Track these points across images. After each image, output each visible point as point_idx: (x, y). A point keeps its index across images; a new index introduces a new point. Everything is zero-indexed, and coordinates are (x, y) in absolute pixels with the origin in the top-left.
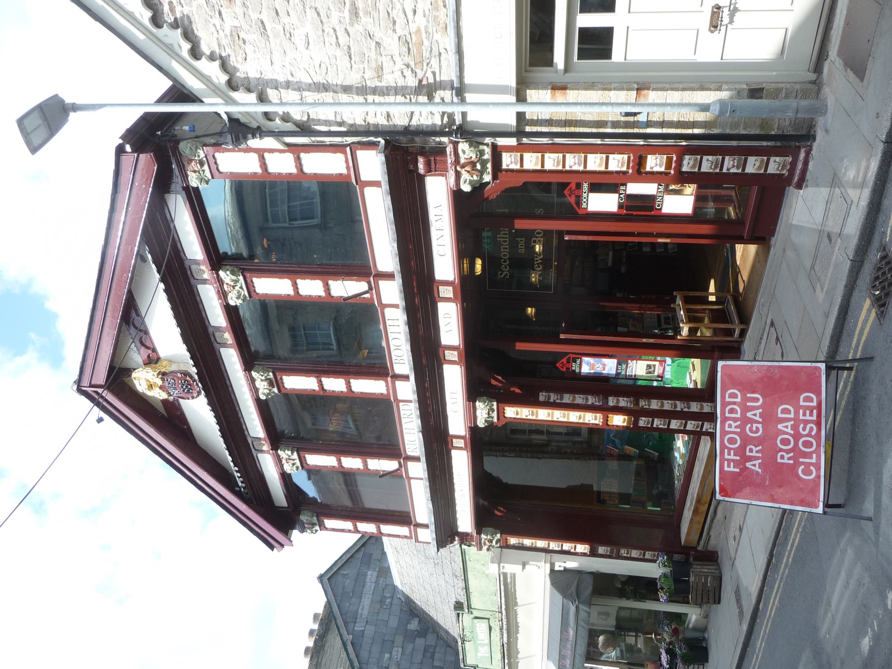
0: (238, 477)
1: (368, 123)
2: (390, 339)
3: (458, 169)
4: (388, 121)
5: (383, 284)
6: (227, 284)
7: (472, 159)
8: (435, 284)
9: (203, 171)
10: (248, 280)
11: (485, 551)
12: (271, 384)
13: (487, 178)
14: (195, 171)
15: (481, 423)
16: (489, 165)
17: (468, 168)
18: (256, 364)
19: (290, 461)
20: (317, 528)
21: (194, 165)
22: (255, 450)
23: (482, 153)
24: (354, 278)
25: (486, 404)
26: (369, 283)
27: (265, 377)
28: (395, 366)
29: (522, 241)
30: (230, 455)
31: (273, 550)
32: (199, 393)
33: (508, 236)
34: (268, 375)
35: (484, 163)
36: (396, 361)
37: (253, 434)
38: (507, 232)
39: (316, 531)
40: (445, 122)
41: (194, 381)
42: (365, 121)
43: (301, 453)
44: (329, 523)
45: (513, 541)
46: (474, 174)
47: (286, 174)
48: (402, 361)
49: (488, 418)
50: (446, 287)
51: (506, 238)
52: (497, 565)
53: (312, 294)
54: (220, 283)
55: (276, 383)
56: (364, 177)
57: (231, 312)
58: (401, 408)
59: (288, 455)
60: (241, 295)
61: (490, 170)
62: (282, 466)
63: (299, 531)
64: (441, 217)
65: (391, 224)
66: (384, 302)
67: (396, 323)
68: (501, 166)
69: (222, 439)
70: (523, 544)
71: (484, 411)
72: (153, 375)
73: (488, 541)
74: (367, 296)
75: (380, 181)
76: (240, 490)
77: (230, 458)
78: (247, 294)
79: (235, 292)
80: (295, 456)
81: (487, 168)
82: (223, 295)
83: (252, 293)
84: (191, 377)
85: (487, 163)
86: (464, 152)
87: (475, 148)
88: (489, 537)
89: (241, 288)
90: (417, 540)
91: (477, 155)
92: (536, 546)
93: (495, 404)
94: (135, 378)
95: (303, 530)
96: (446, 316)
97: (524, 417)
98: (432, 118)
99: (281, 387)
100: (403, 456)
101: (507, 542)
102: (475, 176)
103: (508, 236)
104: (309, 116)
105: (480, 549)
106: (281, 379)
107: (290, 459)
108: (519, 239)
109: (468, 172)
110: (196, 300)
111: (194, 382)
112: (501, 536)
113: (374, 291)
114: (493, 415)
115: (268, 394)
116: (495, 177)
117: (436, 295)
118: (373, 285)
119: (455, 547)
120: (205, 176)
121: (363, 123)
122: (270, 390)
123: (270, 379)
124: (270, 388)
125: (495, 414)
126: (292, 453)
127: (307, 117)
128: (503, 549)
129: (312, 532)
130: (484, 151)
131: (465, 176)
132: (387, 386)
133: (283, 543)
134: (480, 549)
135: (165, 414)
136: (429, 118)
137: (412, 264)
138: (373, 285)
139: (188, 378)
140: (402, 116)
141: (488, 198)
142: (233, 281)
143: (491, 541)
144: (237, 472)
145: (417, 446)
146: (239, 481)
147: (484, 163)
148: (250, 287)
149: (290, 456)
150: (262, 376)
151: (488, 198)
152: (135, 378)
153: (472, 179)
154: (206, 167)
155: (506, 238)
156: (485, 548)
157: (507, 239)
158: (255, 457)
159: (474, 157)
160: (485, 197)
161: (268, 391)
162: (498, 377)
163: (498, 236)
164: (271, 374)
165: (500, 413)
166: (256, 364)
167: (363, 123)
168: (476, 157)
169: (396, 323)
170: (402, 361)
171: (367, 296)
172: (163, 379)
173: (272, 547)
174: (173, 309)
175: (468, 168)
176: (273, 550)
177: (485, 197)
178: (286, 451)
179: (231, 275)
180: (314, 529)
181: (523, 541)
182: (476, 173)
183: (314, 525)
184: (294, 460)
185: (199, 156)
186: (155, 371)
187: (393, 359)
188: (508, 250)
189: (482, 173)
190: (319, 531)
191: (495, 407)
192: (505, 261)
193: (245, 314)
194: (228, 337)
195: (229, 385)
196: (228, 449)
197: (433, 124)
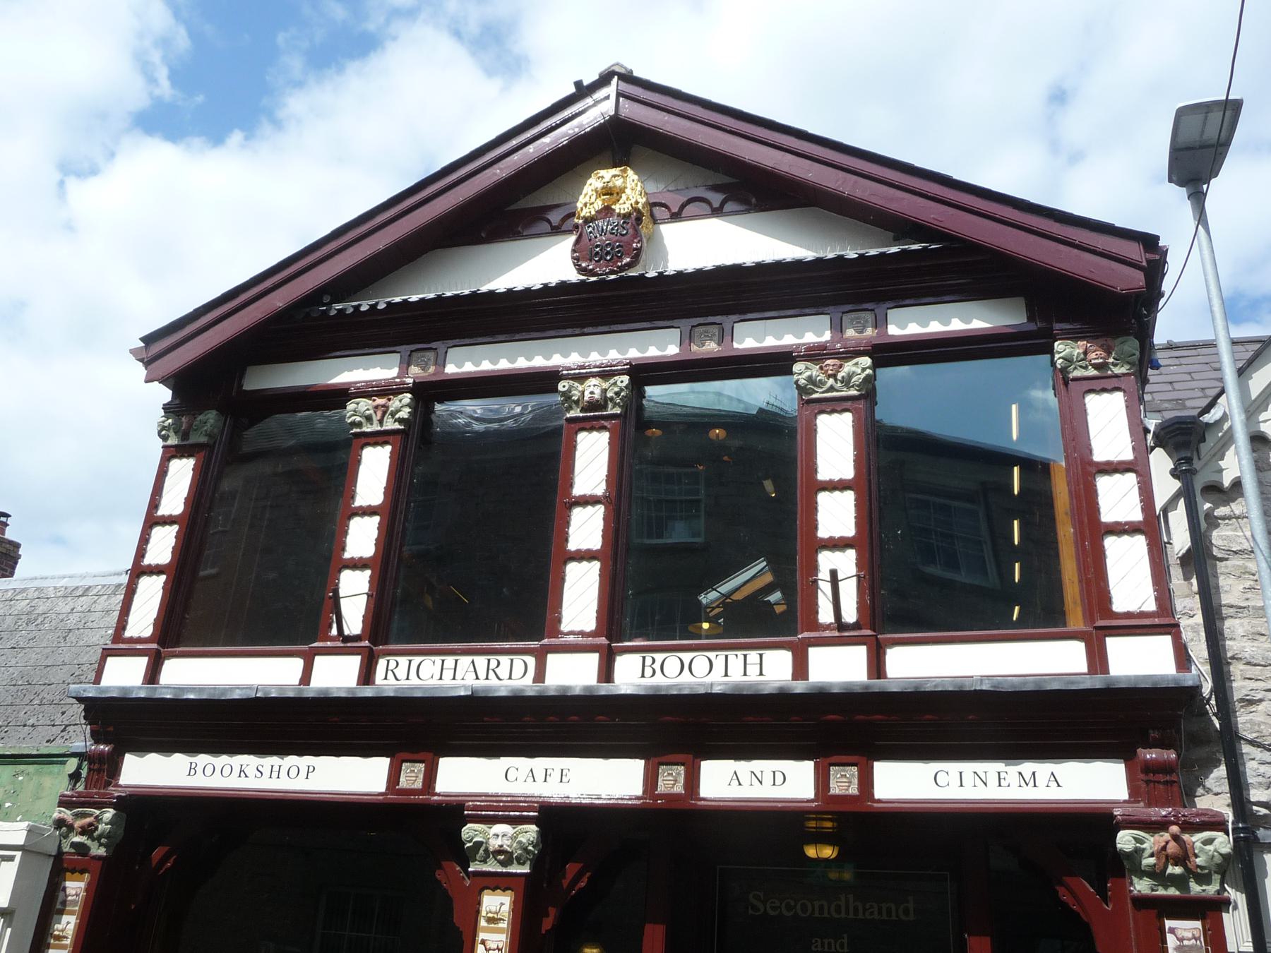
0: (360, 305)
1: (1230, 663)
2: (712, 655)
3: (1175, 829)
4: (1242, 700)
5: (354, 663)
6: (841, 366)
7: (1192, 859)
8: (691, 756)
9: (1085, 368)
10: (848, 404)
11: (56, 815)
12: (593, 406)
13: (1142, 886)
14: (1085, 353)
15: (470, 832)
16: (1173, 892)
17: (1173, 848)
18: (226, 420)
19: (379, 413)
20: (173, 441)
21: (1096, 356)
22: (412, 351)
23: (1204, 879)
24: (868, 598)
25: (530, 848)
26: (856, 626)
27: (611, 399)
28: (636, 659)
29: (842, 946)
30: (422, 300)
31: (142, 339)
32: (581, 270)
33: (851, 916)
34: (615, 405)
35: (1180, 882)
36: (649, 661)
37: (740, 328)
38: (861, 916)
39: (165, 438)
40: (1255, 808)
41: (622, 269)
42: (1233, 658)
43: (399, 437)
44: (182, 472)
45: (75, 887)
46: (1158, 859)
47: (567, 533)
48: (648, 671)
49: (486, 850)
50: (421, 776)
51: (847, 912)
52: (21, 842)
53: (348, 537)
54: (843, 353)
55: (594, 416)
56: (552, 659)
57: (340, 396)
58: (518, 661)
59: (398, 411)
60: (815, 385)
61: (1161, 892)
62: (367, 395)
63: (168, 404)
64: (1032, 783)
65: (1035, 682)
66: (319, 660)
67: (448, 674)
68: (1170, 918)
69: (466, 292)
70: (61, 912)
71: (509, 843)
72: (637, 203)
73: (91, 824)
74: (334, 632)
75: (99, 684)
76: (324, 305)
77: (414, 298)
78: (815, 396)
79: (822, 377)
80: (390, 425)
81: (1166, 888)
82: (369, 391)
83: (817, 407)
84: (630, 266)
85: (1178, 889)
86: (1209, 841)
87: (1218, 865)
88: (102, 827)
89: (832, 389)
90: (107, 653)
91: (1201, 867)
92: (48, 946)
93: (525, 869)
94: (625, 171)
95: (167, 408)
96: (311, 769)
97: (482, 936)
98: (1260, 784)
99: (582, 425)
100: (374, 648)
101: (73, 871)
102: (1152, 860)
103: (851, 916)
104: (1222, 560)
105: (64, 803)
106: (603, 428)
107: (384, 413)
108: (845, 941)
109: (1164, 848)
110: (925, 296)
111: (618, 267)
112: (94, 858)
113: (340, 644)
114: (491, 861)
115: (570, 397)
116: (1142, 902)
117: (834, 759)
118: (349, 645)
119: (81, 740)
120: (1075, 368)
121: (1229, 655)
122: (577, 402)
123: (605, 407)
124: (581, 405)
125: (492, 867)
126: (400, 421)
127: (1220, 556)
128: (51, 861)
129: (163, 428)
130: (1209, 882)
131: (1152, 842)
132: (140, 640)
133: (154, 365)
134: (64, 803)
135: (513, 207)
136: (1260, 779)
137: (927, 717)
138: (349, 645)
139: (627, 260)
140: (1257, 728)
141: (440, 867)
142: (850, 376)
143: (87, 831)
144: (373, 307)
145: (403, 682)
146: (348, 306)
147: (1180, 882)
148: (378, 438)
149: (393, 414)
150: (617, 394)
151: (440, 867)
152: (625, 171)
153: (1146, 854)
154: (1092, 372)
155: (847, 912)
156: (67, 814)
157: (843, 915)
158: (711, 319)
159: (1199, 861)
160: (444, 863)
161: (575, 398)
162: (585, 879)
163: (851, 897)
164: (618, 411)
165: (497, 882)
166: (226, 420)
167: (1229, 655)
168: (1198, 866)
169: (448, 674)
170: (648, 671)
171: (334, 632)
172: (626, 216)
173: (149, 340)
174: (700, 273)
175: (1173, 848)
176: (142, 339)
177: (444, 863)
178: (408, 410)
179: (863, 376)
180: (172, 434)
181: (72, 913)
182: (1161, 865)
183: (185, 435)
184: (381, 422)
185: (1115, 365)
186: (643, 208)
187: (657, 656)
188: (817, 914)
189: (1157, 875)
190: (161, 443)
191: (516, 869)
192: (789, 908)
193: (321, 419)
194: (711, 348)
195: (586, 330)
196: (440, 298)
197: (1248, 785)
